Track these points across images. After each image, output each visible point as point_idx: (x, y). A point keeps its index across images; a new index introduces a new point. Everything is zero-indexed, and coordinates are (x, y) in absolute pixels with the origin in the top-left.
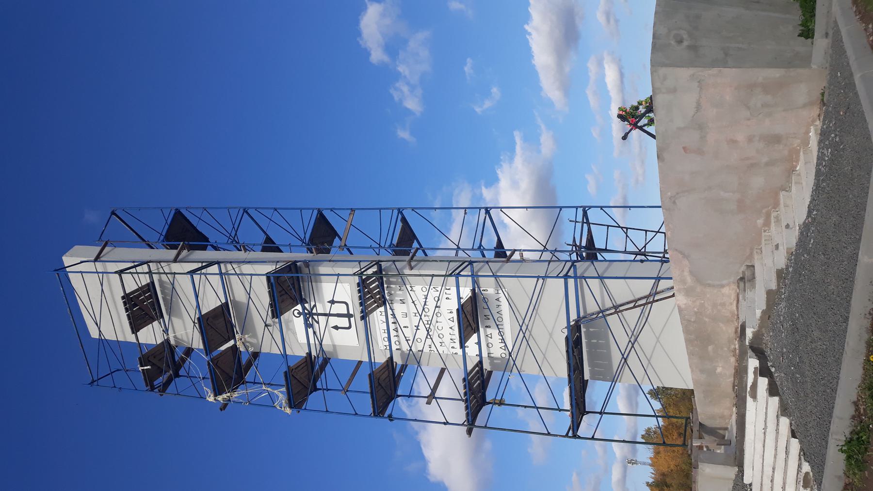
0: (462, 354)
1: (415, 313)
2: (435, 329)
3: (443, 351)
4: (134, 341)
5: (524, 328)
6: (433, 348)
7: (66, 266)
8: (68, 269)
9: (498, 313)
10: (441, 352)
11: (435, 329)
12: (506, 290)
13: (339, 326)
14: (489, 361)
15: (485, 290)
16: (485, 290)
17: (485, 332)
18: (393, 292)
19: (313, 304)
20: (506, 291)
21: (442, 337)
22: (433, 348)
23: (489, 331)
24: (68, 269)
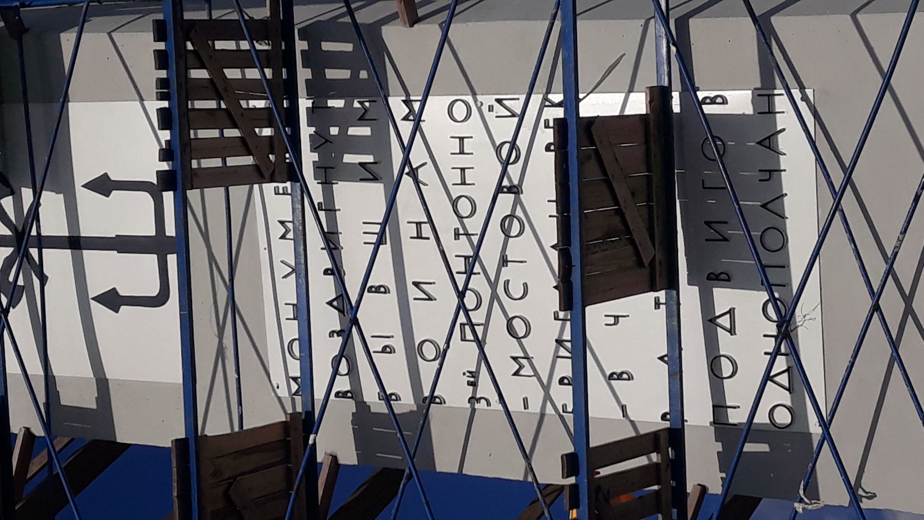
0: (181, 381)
1: (419, 224)
2: (494, 296)
3: (525, 401)
4: (385, 410)
5: (892, 303)
6: (485, 388)
7: (44, 250)
8: (569, 355)
9: (764, 206)
10: (515, 406)
11: (494, 296)
12: (809, 92)
13: (122, 293)
14: (719, 447)
15: (713, 101)
16: (713, 101)
17: (707, 303)
18: (334, 131)
19: (27, 195)
20: (805, 98)
21: (521, 331)
22: (485, 388)
23: (723, 297)
24: (569, 355)
